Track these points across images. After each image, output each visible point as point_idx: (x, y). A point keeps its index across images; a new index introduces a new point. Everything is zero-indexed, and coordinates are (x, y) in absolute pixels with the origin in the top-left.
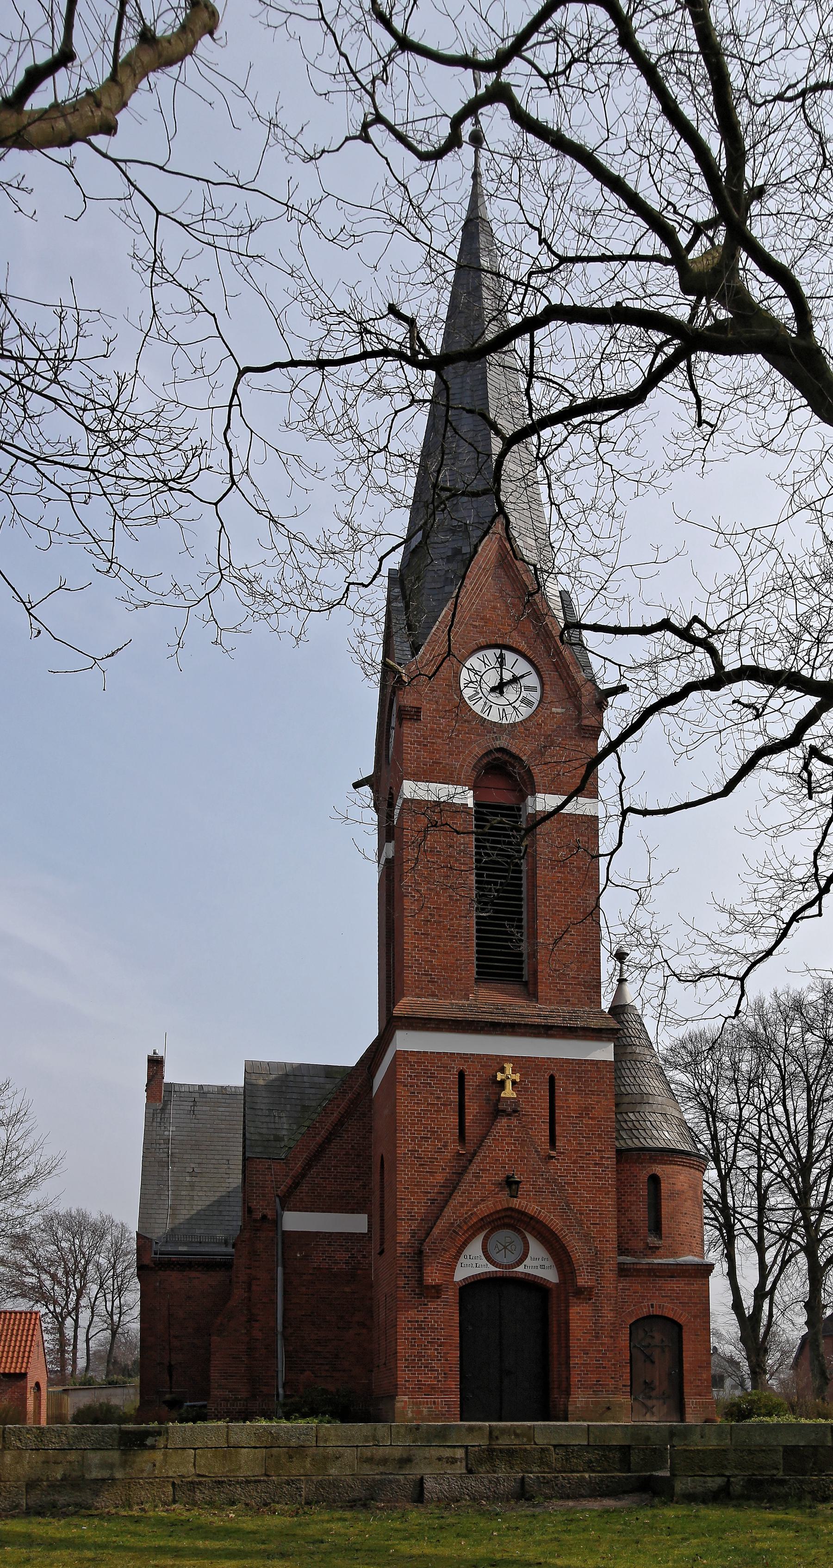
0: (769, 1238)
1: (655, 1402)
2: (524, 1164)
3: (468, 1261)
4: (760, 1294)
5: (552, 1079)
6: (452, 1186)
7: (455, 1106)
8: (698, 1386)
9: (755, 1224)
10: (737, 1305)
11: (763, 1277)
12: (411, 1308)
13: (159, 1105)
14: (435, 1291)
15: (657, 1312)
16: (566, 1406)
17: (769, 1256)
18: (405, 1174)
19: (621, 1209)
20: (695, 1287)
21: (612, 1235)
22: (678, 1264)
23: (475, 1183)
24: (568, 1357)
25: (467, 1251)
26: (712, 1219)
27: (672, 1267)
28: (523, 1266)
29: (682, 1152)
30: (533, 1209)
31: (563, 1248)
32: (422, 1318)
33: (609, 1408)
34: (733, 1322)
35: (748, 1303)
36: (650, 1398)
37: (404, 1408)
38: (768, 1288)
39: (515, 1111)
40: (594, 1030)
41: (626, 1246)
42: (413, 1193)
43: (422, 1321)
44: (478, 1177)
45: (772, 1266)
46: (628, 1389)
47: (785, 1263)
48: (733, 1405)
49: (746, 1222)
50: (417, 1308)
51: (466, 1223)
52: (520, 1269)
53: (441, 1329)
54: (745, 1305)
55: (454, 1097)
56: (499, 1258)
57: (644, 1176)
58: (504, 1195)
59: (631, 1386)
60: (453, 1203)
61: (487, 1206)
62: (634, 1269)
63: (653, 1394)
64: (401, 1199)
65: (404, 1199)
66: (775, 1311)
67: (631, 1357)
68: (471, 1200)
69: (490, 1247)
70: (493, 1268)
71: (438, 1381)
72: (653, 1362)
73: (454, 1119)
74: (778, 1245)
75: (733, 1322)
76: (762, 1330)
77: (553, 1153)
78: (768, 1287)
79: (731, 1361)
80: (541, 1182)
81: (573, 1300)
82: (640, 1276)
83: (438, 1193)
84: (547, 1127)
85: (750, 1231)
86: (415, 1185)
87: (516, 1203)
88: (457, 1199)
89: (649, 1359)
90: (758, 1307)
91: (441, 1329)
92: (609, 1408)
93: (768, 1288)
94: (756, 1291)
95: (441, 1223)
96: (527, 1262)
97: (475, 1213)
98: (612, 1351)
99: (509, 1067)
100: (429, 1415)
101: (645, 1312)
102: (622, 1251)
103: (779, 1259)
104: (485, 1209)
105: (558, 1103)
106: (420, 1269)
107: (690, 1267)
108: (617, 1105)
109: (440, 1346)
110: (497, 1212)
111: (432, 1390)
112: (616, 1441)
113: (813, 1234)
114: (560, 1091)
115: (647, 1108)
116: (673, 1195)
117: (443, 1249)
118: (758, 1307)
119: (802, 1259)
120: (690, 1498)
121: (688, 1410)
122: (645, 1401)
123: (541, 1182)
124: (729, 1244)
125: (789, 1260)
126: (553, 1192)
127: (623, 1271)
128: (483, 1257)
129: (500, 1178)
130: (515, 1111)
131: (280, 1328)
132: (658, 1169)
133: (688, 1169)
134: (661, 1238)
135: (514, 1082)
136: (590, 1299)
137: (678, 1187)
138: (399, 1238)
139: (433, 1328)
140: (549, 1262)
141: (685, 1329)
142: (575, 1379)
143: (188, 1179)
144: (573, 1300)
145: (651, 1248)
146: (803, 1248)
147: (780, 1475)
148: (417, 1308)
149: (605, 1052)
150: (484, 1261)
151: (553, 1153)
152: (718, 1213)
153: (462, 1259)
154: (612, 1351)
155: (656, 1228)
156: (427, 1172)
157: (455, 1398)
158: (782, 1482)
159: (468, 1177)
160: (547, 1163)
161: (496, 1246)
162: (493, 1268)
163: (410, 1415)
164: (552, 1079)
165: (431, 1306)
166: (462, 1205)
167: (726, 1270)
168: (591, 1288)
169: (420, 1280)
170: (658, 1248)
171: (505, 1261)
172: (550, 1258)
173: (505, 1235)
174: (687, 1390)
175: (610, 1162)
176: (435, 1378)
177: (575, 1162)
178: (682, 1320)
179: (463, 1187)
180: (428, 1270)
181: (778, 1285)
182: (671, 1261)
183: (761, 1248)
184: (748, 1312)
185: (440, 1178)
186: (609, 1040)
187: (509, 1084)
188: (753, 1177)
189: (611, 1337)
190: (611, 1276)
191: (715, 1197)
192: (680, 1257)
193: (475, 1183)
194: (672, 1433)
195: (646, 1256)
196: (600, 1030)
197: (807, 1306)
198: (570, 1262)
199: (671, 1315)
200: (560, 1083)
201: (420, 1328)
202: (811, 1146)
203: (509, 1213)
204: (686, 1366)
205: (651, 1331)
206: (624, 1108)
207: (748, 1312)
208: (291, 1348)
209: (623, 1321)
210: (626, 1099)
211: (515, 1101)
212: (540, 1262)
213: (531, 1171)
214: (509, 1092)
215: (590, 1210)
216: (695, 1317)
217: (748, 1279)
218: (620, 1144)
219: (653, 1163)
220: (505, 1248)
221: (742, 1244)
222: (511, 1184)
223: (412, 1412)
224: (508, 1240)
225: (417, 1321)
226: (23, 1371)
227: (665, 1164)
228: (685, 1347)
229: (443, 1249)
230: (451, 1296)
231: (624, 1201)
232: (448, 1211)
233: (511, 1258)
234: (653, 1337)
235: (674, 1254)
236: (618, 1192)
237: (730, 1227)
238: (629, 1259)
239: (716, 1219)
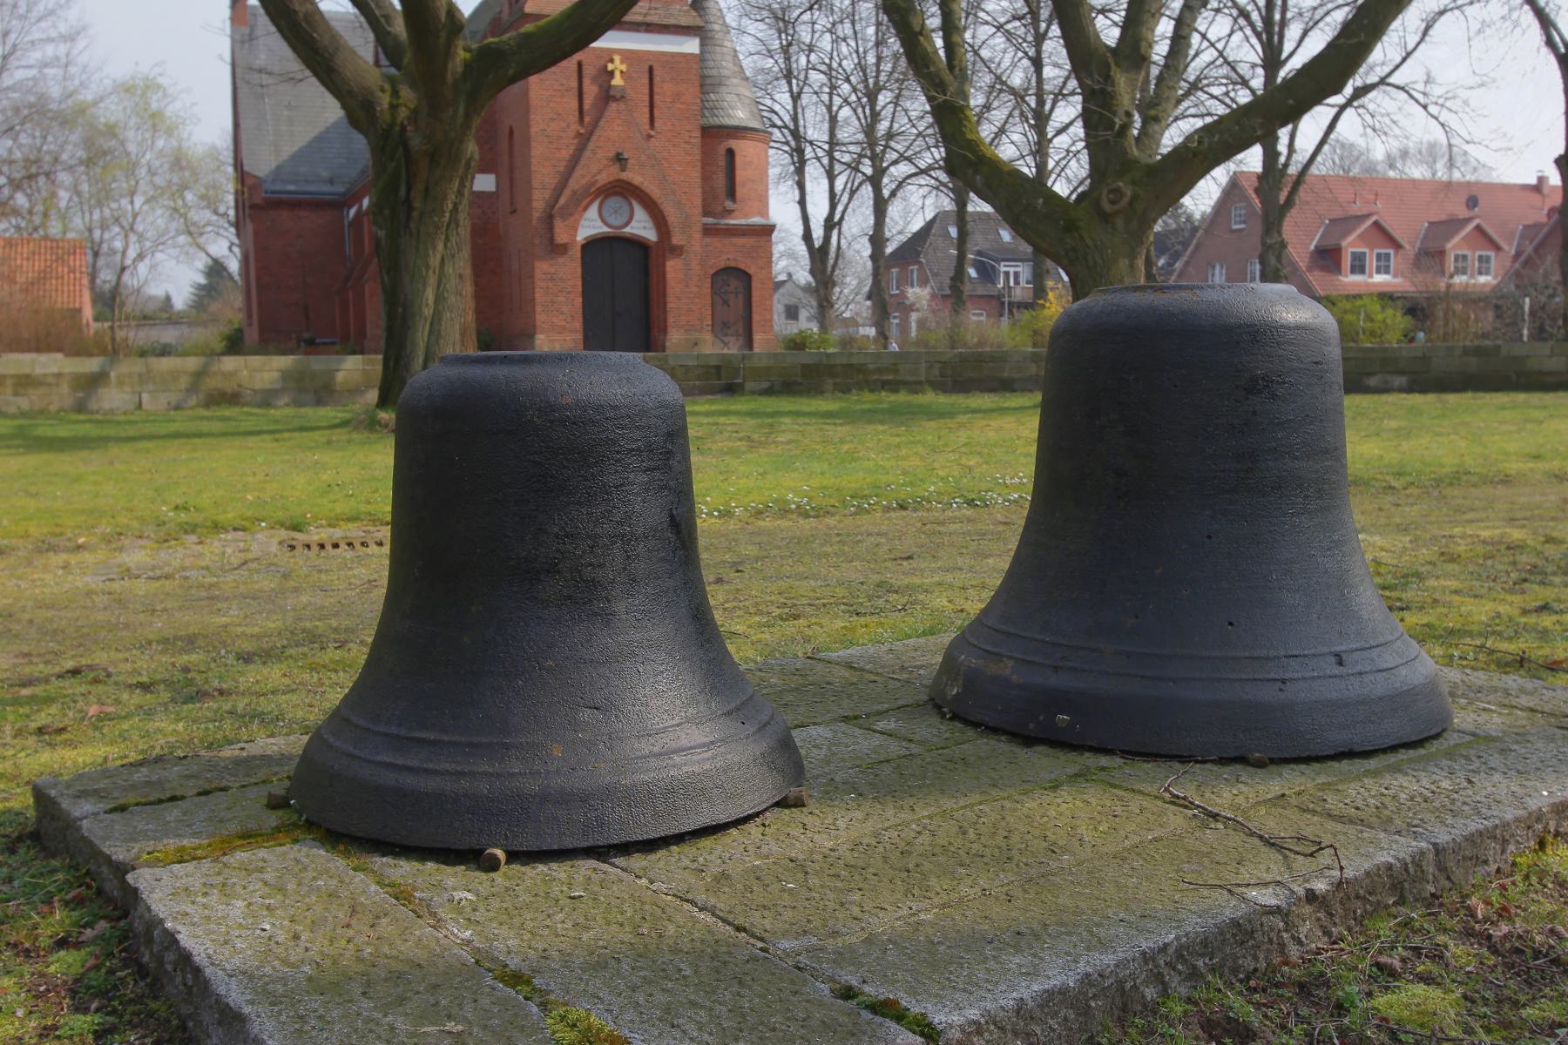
0: (838, 168)
4: (830, 224)
5: (651, 69)
6: (575, 161)
7: (575, 92)
10: (807, 236)
11: (833, 206)
13: (246, 30)
14: (562, 249)
15: (733, 264)
16: (664, 342)
17: (839, 183)
19: (706, 178)
21: (698, 202)
24: (665, 303)
29: (752, 129)
30: (637, 180)
31: (661, 212)
32: (552, 270)
35: (818, 233)
36: (726, 335)
39: (623, 97)
40: (683, 27)
44: (594, 153)
47: (853, 193)
48: (791, 340)
52: (628, 230)
55: (575, 84)
57: (722, 149)
58: (615, 169)
66: (843, 241)
70: (606, 229)
73: (574, 104)
76: (831, 262)
77: (652, 133)
78: (837, 218)
80: (643, 158)
84: (647, 110)
87: (625, 176)
88: (579, 172)
89: (726, 302)
90: (827, 238)
95: (567, 192)
96: (633, 223)
99: (617, 58)
101: (722, 265)
102: (706, 214)
103: (849, 185)
104: (603, 179)
105: (656, 89)
108: (702, 86)
111: (562, 330)
112: (713, 362)
114: (657, 79)
115: (718, 49)
118: (827, 238)
119: (867, 191)
120: (753, 393)
121: (756, 345)
127: (708, 231)
129: (612, 154)
130: (623, 97)
132: (734, 144)
135: (622, 72)
138: (535, 204)
140: (650, 224)
142: (670, 320)
143: (285, 113)
147: (799, 380)
149: (691, 46)
150: (599, 223)
151: (652, 133)
152: (790, 138)
155: (731, 193)
157: (580, 336)
158: (800, 384)
159: (587, 153)
164: (651, 69)
165: (561, 260)
166: (583, 176)
167: (797, 198)
168: (681, 247)
169: (552, 239)
171: (616, 223)
173: (614, 202)
175: (697, 134)
177: (669, 141)
178: (751, 271)
179: (583, 161)
182: (743, 222)
183: (831, 177)
184: (817, 244)
186: (695, 35)
187: (617, 74)
190: (697, 235)
191: (787, 118)
194: (744, 357)
195: (723, 217)
196: (688, 28)
198: (655, 203)
199: (742, 267)
200: (657, 73)
201: (552, 279)
206: (708, 88)
207: (817, 244)
210: (708, 81)
211: (623, 89)
214: (617, 81)
217: (819, 209)
218: (704, 121)
221: (814, 172)
222: (619, 159)
226: (77, 306)
230: (576, 252)
235: (746, 216)
237: (800, 151)
238: (710, 220)
239: (787, 143)
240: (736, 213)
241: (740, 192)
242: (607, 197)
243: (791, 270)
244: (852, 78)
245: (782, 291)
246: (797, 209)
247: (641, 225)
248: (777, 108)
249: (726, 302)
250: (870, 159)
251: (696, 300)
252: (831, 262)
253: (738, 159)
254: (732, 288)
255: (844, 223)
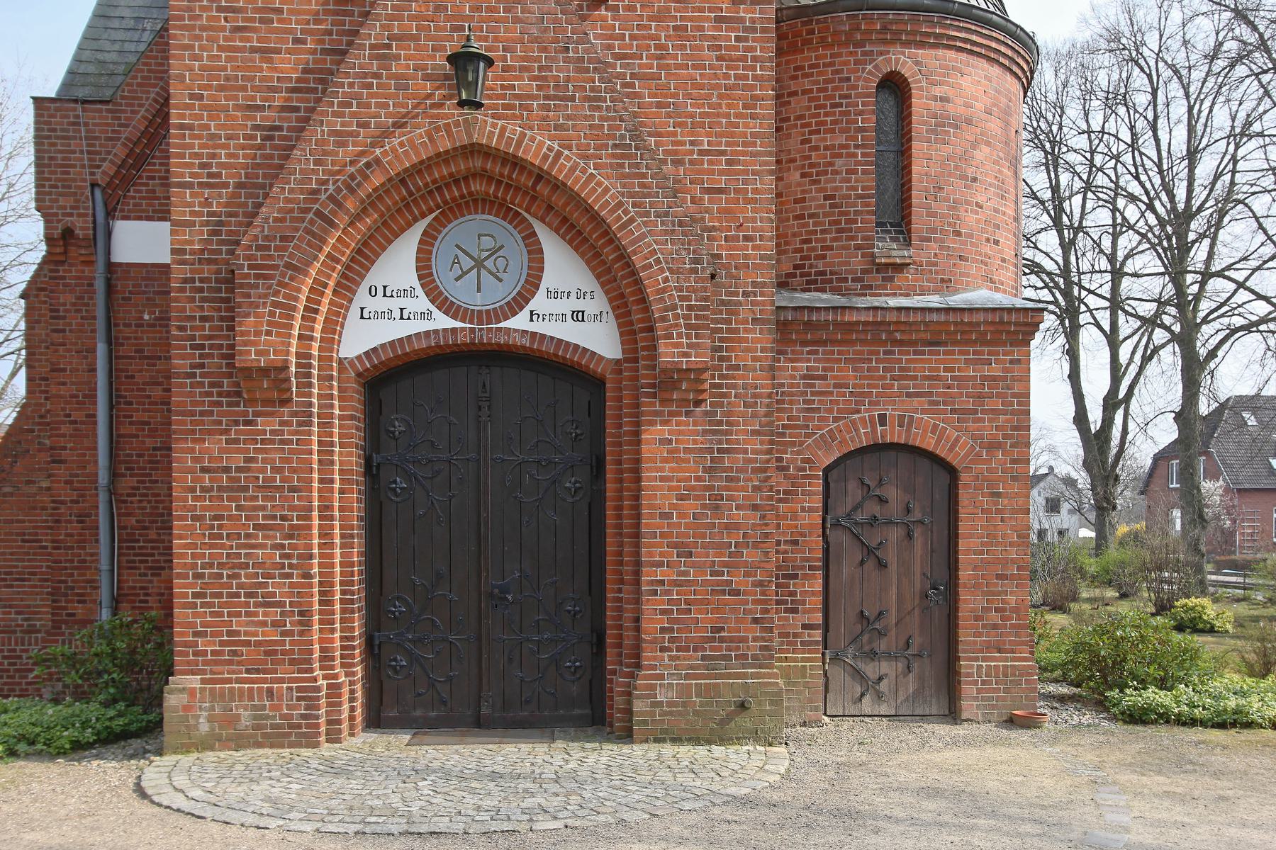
0: (1127, 326)
1: (885, 667)
2: (517, 20)
3: (379, 303)
4: (1111, 403)
8: (995, 626)
9: (1107, 304)
10: (1081, 419)
11: (1116, 378)
12: (210, 432)
15: (894, 434)
17: (1124, 352)
18: (195, 58)
20: (995, 369)
22: (948, 310)
23: (377, 76)
25: (380, 274)
26: (1051, 303)
27: (935, 317)
28: (525, 314)
31: (624, 258)
33: (742, 706)
34: (1075, 440)
35: (1095, 416)
36: (873, 655)
37: (187, 708)
38: (1121, 395)
41: (820, 265)
42: (214, 111)
43: (239, 470)
45: (1128, 365)
46: (818, 635)
47: (1146, 359)
49: (1092, 301)
50: (227, 432)
51: (352, 191)
52: (519, 322)
53: (293, 489)
54: (1091, 419)
56: (463, 293)
57: (868, 78)
59: (826, 627)
60: (318, 132)
61: (411, 141)
62: (837, 325)
63: (882, 645)
64: (182, 127)
65: (191, 127)
66: (1132, 426)
67: (826, 551)
68: (366, 125)
69: (440, 265)
70: (443, 322)
71: (284, 634)
72: (882, 565)
74: (1136, 338)
75: (1075, 440)
79: (1070, 482)
81: (649, 405)
82: (852, 343)
83: (283, 109)
85: (1098, 315)
86: (221, 88)
89: (873, 556)
90: (1108, 422)
91: (293, 489)
92: (742, 706)
93: (1121, 395)
94: (1106, 399)
95: (285, 193)
96: (539, 302)
97: (377, 161)
98: (756, 545)
100: (257, 727)
101: (863, 437)
106: (230, 322)
107: (981, 317)
109: (291, 537)
110: (443, 158)
113: (1190, 315)
116: (945, 124)
117: (288, 266)
118: (1108, 422)
121: (968, 690)
122: (860, 665)
123: (560, 70)
124: (1072, 334)
125: (1151, 358)
126: (594, 100)
128: (419, 291)
131: (103, 477)
133: (983, 63)
134: (908, 243)
136: (698, 403)
137: (956, 108)
139: (268, 487)
140: (597, 304)
141: (965, 478)
142: (653, 625)
144: (649, 405)
145: (882, 268)
146: (1174, 338)
148: (227, 432)
150: (422, 303)
153: (362, 297)
154: (756, 545)
156: (253, 50)
159: (361, 58)
160: (583, 18)
161: (456, 261)
162: (443, 322)
163: (204, 727)
166: (342, 138)
170: (899, 268)
171: (478, 302)
172: (599, 292)
174: (965, 635)
176: (274, 624)
179: (345, 85)
180: (247, 324)
181: (1136, 391)
182: (933, 301)
183: (1113, 341)
185: (289, 66)
188: (1106, 243)
189: (755, 507)
190: (759, 338)
192: (956, 291)
193: (377, 76)
195: (867, 289)
197: (1179, 417)
199: (929, 443)
201: (236, 489)
202: (1189, 197)
203: (478, 163)
204: (965, 574)
205: (880, 483)
208: (133, 520)
209: (808, 461)
212: (574, 304)
213: (534, 40)
215: (701, 152)
216: (992, 447)
217: (1096, 384)
219: (892, 42)
220: (479, 264)
223: (210, 720)
224: (487, 242)
225: (227, 470)
227: (921, 45)
228: (963, 526)
229: (288, 266)
231: (816, 148)
232: (302, 158)
233: (495, 294)
234: (882, 501)
236: (781, 99)
239: (1056, 303)
240: (909, 274)
241: (919, 220)
242: (451, 211)
243: (1053, 463)
244: (1157, 204)
245: (1042, 484)
246: (1067, 388)
247: (566, 306)
248: (1040, 258)
249: (873, 556)
250: (1176, 306)
251: (748, 556)
252: (1114, 451)
253: (919, 103)
254: (894, 509)
255: (1134, 401)
